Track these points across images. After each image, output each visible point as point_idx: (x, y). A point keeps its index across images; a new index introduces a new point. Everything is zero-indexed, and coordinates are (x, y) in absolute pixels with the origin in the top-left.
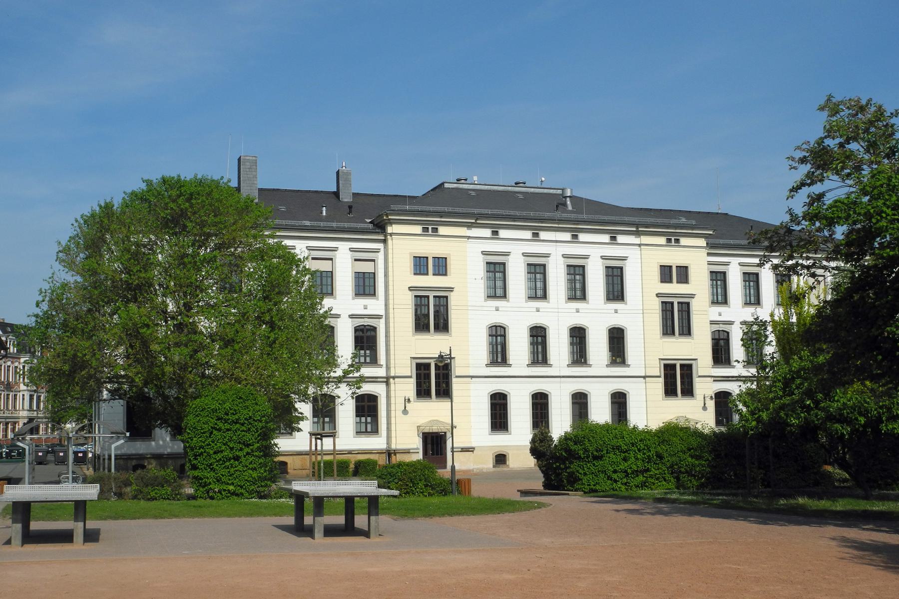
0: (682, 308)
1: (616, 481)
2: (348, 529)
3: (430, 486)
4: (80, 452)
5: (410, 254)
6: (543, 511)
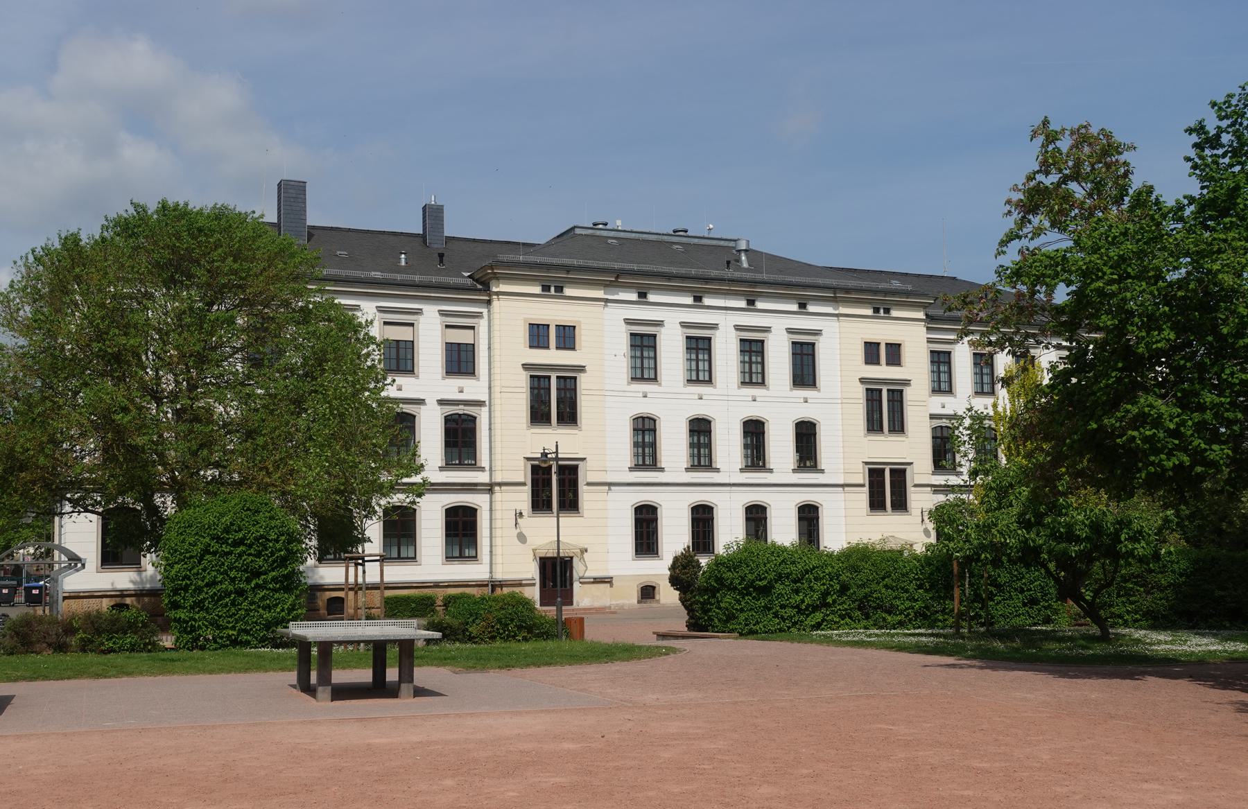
0: (893, 397)
1: (783, 619)
2: (379, 689)
3: (525, 628)
4: (36, 588)
5: (525, 320)
6: (659, 662)
